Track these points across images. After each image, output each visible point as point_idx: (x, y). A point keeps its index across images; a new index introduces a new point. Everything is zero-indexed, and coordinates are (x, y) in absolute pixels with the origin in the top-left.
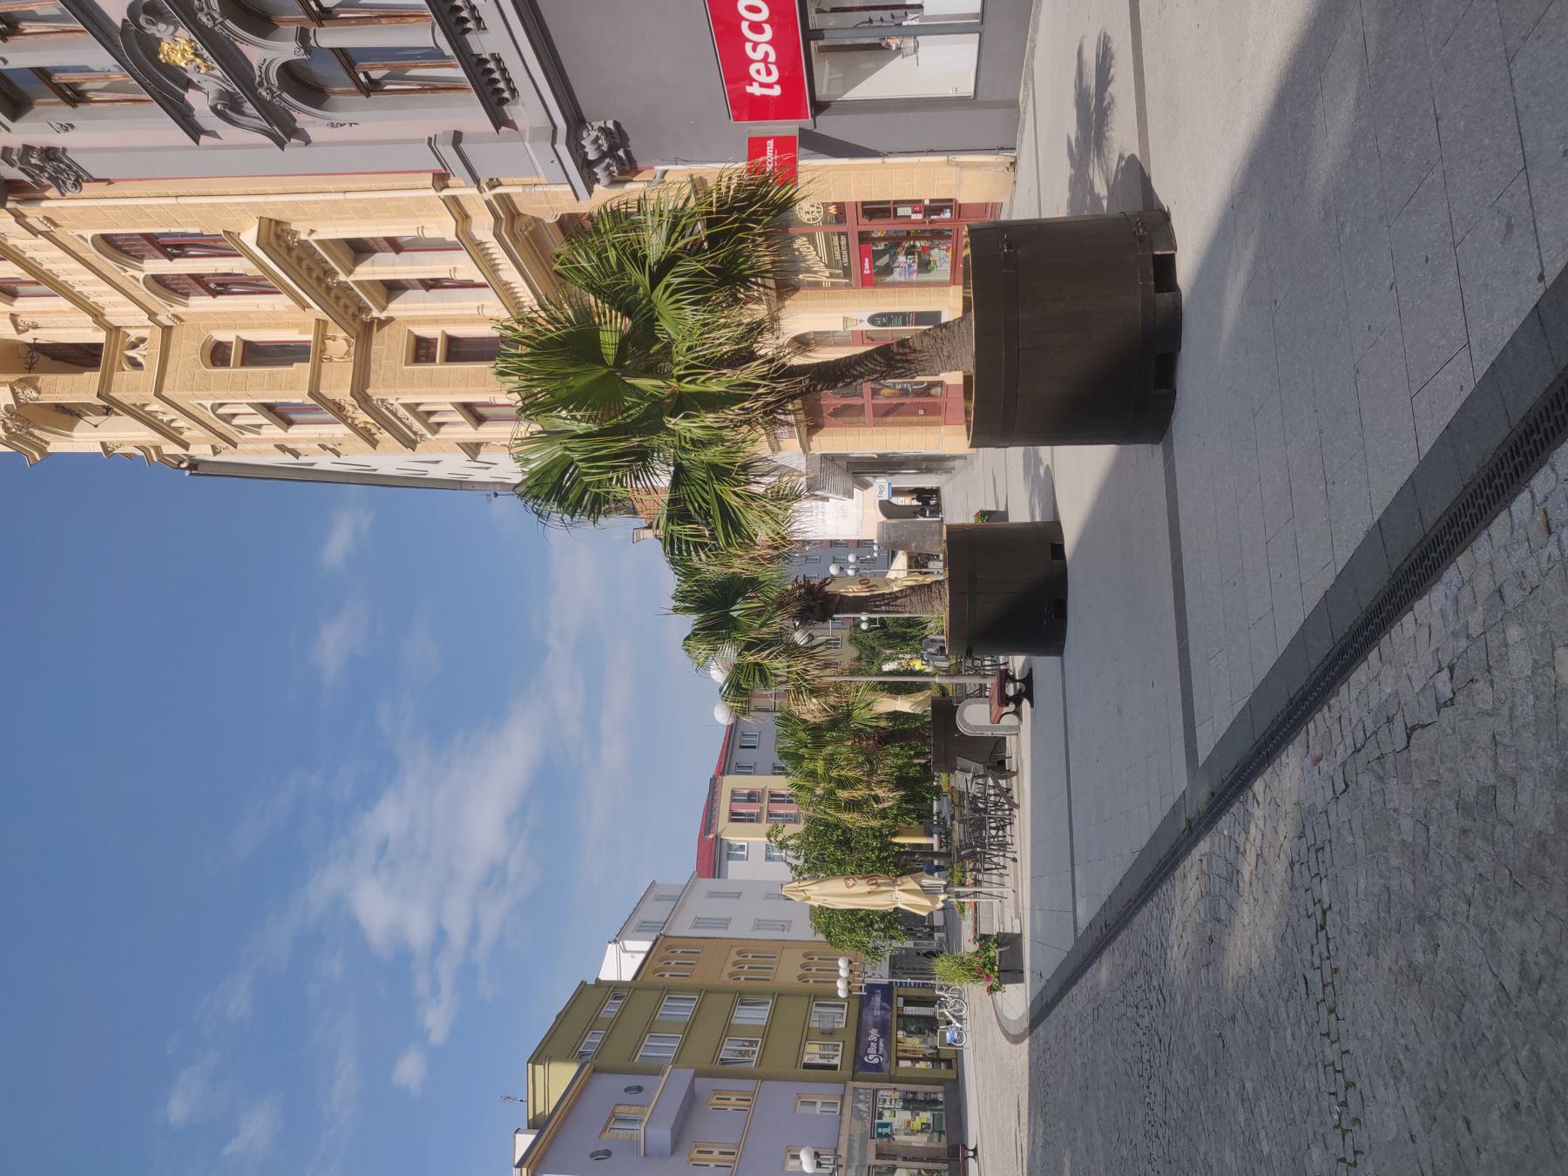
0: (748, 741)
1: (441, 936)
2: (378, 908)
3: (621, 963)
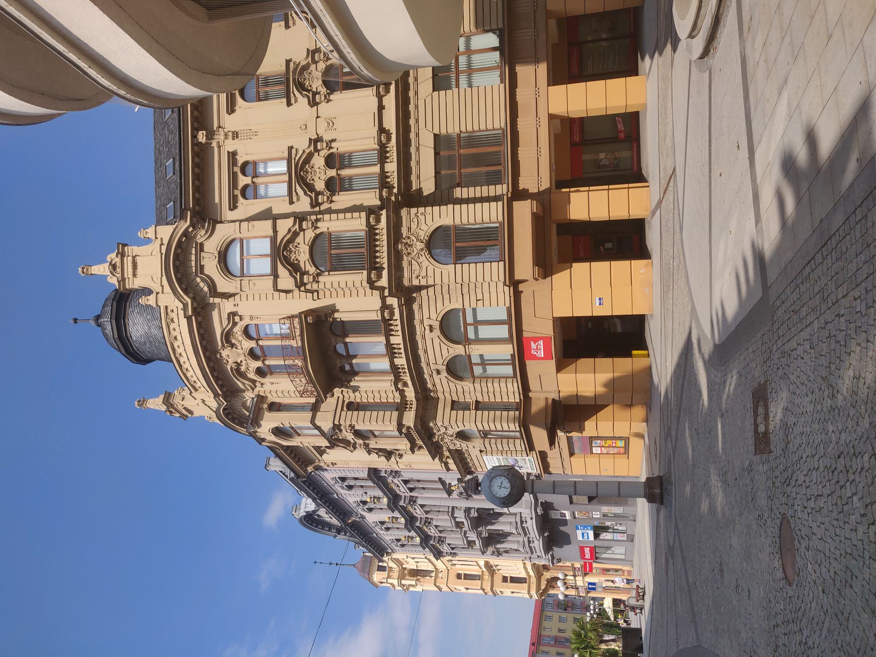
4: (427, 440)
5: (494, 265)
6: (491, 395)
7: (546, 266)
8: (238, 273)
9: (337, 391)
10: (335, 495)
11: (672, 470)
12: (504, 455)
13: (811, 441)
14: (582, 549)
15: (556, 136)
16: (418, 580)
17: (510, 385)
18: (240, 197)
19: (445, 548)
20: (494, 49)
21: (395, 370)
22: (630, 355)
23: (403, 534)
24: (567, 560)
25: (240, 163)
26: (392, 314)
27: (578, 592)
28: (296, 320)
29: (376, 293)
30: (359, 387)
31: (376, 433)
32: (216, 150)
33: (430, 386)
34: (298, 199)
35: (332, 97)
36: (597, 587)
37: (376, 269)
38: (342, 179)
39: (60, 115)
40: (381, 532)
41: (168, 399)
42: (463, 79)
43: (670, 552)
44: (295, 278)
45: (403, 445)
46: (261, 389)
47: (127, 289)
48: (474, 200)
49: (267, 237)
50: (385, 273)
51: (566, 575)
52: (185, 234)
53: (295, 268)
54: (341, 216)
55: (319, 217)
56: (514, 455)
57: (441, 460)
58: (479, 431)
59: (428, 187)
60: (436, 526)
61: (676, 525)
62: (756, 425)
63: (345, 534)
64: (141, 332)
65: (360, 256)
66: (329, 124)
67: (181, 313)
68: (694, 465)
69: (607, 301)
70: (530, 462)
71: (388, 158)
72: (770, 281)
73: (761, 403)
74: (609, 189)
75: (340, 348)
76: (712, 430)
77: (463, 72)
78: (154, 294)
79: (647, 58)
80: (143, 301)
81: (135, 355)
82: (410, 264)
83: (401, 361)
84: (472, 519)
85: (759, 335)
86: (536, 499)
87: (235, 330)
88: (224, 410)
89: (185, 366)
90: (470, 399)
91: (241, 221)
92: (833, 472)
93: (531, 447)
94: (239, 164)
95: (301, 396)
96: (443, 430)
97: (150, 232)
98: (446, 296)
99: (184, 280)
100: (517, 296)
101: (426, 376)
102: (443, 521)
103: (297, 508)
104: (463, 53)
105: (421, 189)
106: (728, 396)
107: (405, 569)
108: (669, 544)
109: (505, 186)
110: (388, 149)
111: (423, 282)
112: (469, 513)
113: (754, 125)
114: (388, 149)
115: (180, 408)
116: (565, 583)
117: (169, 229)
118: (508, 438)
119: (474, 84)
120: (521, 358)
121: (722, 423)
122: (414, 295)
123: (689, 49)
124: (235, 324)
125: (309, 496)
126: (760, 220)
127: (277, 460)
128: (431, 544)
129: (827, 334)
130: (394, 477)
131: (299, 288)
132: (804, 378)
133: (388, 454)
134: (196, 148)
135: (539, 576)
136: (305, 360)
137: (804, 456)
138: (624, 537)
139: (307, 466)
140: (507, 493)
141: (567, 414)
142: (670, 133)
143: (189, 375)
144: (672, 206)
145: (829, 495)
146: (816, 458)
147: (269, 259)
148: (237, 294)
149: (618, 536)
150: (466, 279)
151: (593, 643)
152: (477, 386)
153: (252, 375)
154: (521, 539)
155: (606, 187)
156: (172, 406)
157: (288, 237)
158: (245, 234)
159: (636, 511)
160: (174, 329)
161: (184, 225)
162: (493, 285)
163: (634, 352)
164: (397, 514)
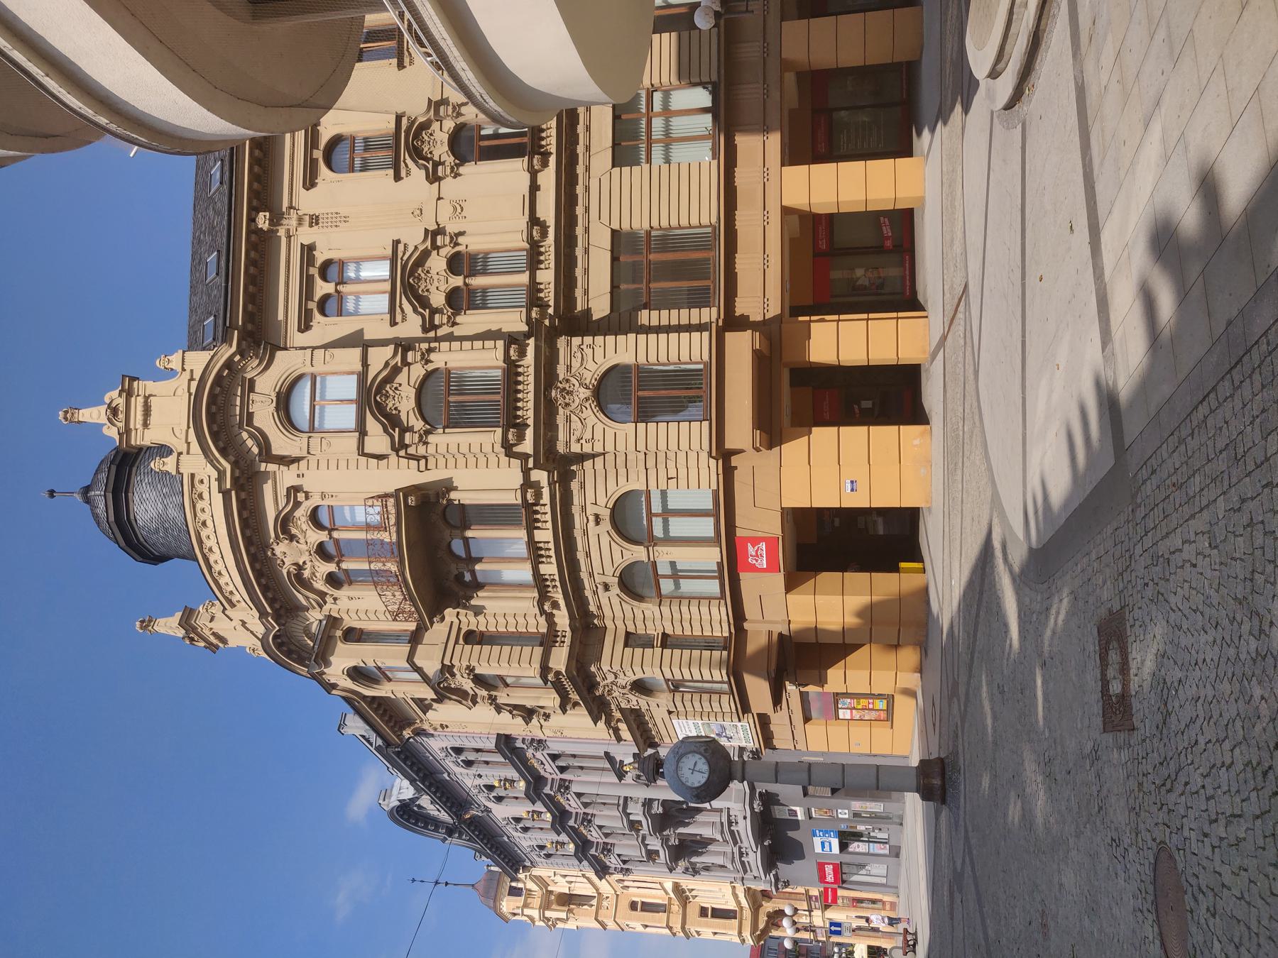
4: (585, 693)
5: (695, 425)
6: (687, 625)
7: (772, 430)
8: (306, 427)
9: (450, 613)
10: (445, 775)
11: (960, 748)
12: (705, 718)
13: (1216, 715)
14: (821, 867)
15: (792, 240)
16: (570, 911)
17: (715, 610)
18: (316, 312)
19: (613, 861)
20: (705, 110)
21: (540, 582)
22: (896, 569)
23: (549, 838)
24: (798, 884)
25: (318, 263)
26: (538, 495)
27: (816, 936)
28: (391, 501)
29: (516, 463)
30: (483, 607)
31: (509, 681)
32: (284, 240)
33: (593, 608)
34: (404, 319)
35: (462, 170)
36: (843, 930)
37: (515, 426)
38: (471, 292)
39: (14, 159)
40: (515, 834)
41: (187, 620)
42: (657, 152)
43: (957, 878)
44: (392, 437)
45: (550, 699)
46: (333, 606)
47: (133, 447)
48: (668, 329)
49: (352, 373)
50: (529, 433)
51: (796, 910)
52: (229, 364)
53: (392, 421)
54: (467, 344)
55: (433, 345)
56: (720, 719)
57: (608, 723)
58: (667, 681)
59: (600, 307)
60: (600, 827)
61: (967, 838)
62: (1105, 683)
63: (460, 837)
64: (152, 512)
65: (493, 407)
66: (455, 209)
67: (215, 485)
68: (995, 743)
69: (862, 486)
71: (541, 262)
72: (1128, 441)
73: (1114, 644)
74: (868, 319)
75: (458, 547)
76: (1026, 689)
77: (658, 141)
78: (175, 455)
79: (926, 133)
80: (156, 465)
81: (142, 550)
82: (568, 420)
83: (549, 569)
84: (653, 817)
85: (1109, 530)
86: (752, 788)
87: (298, 514)
88: (275, 637)
89: (216, 568)
90: (654, 630)
91: (314, 348)
92: (1265, 774)
93: (745, 707)
94: (318, 264)
95: (395, 620)
96: (611, 678)
97: (175, 361)
98: (622, 471)
99: (223, 436)
100: (728, 473)
101: (588, 593)
102: (609, 818)
103: (386, 794)
104: (659, 115)
105: (589, 310)
106: (1054, 633)
107: (551, 892)
108: (955, 869)
109: (714, 310)
110: (542, 250)
111: (587, 449)
112: (650, 807)
113: (1099, 188)
114: (542, 250)
115: (207, 633)
116: (794, 923)
117: (204, 356)
118: (711, 692)
119: (674, 160)
120: (732, 568)
121: (1043, 676)
122: (574, 468)
123: (991, 96)
124: (297, 504)
125: (407, 776)
126: (1111, 340)
127: (357, 718)
128: (592, 854)
129: (1245, 520)
130: (536, 749)
131: (397, 451)
132: (1197, 599)
133: (528, 713)
134: (253, 237)
135: (756, 908)
136: (401, 563)
137: (1202, 741)
138: (885, 850)
140: (703, 781)
141: (801, 658)
142: (959, 234)
143: (222, 581)
144: (962, 342)
145: (1258, 817)
146: (1227, 745)
147: (354, 407)
148: (303, 458)
149: (876, 849)
150: (652, 446)
152: (665, 610)
153: (320, 585)
154: (728, 849)
155: (865, 316)
156: (194, 630)
157: (384, 373)
158: (319, 368)
159: (903, 810)
160: (203, 510)
161: (227, 352)
162: (692, 456)
163: (903, 565)
164: (539, 807)
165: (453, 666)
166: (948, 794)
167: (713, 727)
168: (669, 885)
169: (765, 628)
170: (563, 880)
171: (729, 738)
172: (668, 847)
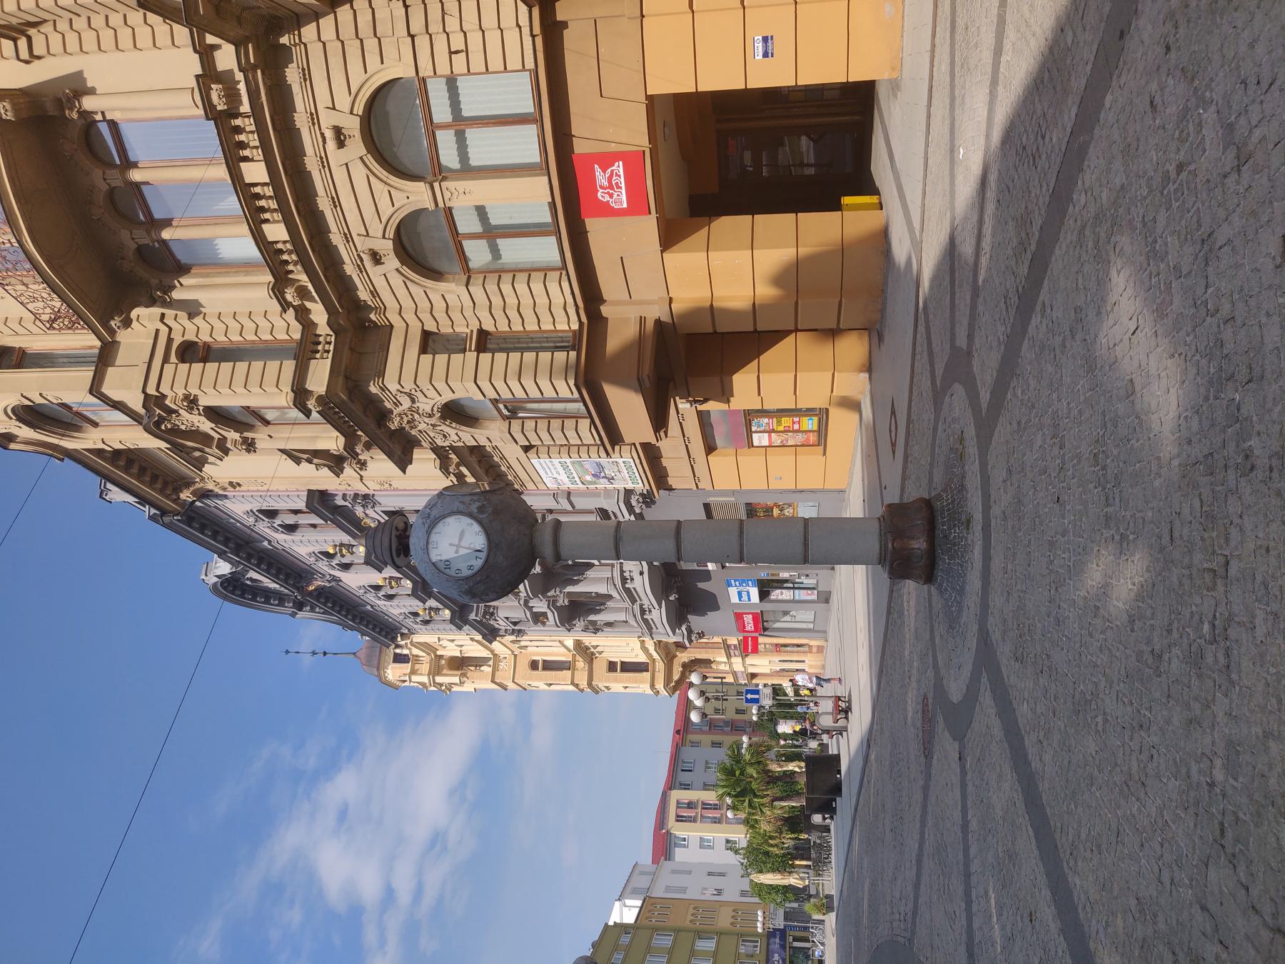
0: (687, 766)
1: (389, 895)
2: (344, 868)
3: (626, 912)
4: (373, 426)
10: (266, 543)
12: (574, 455)
14: (739, 617)
16: (464, 675)
17: (553, 288)
22: (837, 207)
23: (416, 605)
26: (232, 95)
31: (270, 416)
33: (363, 295)
40: (379, 602)
63: (312, 610)
69: (783, 47)
70: (629, 468)
90: (465, 327)
93: (612, 436)
98: (371, 44)
101: (349, 269)
107: (441, 657)
122: (284, 40)
135: (669, 658)
138: (813, 596)
139: (178, 490)
141: (690, 358)
151: (754, 785)
152: (477, 290)
163: (846, 200)
165: (164, 396)
166: (940, 565)
167: (587, 466)
168: (570, 643)
169: (633, 313)
170: (452, 645)
171: (611, 479)
172: (557, 608)
